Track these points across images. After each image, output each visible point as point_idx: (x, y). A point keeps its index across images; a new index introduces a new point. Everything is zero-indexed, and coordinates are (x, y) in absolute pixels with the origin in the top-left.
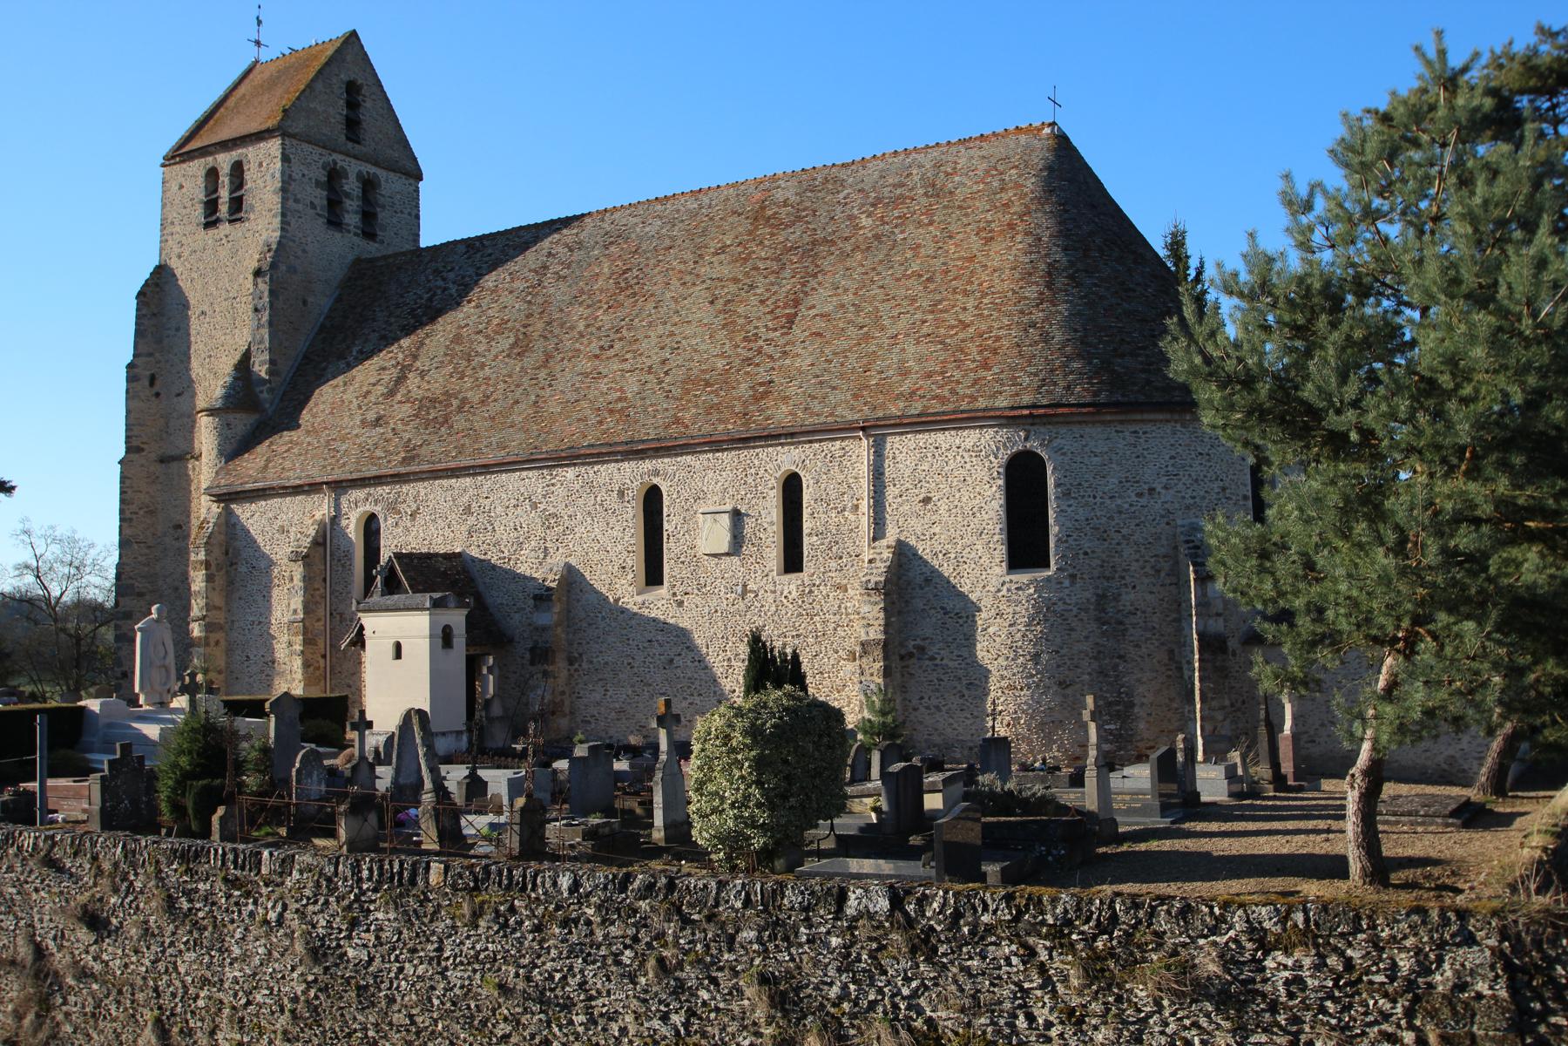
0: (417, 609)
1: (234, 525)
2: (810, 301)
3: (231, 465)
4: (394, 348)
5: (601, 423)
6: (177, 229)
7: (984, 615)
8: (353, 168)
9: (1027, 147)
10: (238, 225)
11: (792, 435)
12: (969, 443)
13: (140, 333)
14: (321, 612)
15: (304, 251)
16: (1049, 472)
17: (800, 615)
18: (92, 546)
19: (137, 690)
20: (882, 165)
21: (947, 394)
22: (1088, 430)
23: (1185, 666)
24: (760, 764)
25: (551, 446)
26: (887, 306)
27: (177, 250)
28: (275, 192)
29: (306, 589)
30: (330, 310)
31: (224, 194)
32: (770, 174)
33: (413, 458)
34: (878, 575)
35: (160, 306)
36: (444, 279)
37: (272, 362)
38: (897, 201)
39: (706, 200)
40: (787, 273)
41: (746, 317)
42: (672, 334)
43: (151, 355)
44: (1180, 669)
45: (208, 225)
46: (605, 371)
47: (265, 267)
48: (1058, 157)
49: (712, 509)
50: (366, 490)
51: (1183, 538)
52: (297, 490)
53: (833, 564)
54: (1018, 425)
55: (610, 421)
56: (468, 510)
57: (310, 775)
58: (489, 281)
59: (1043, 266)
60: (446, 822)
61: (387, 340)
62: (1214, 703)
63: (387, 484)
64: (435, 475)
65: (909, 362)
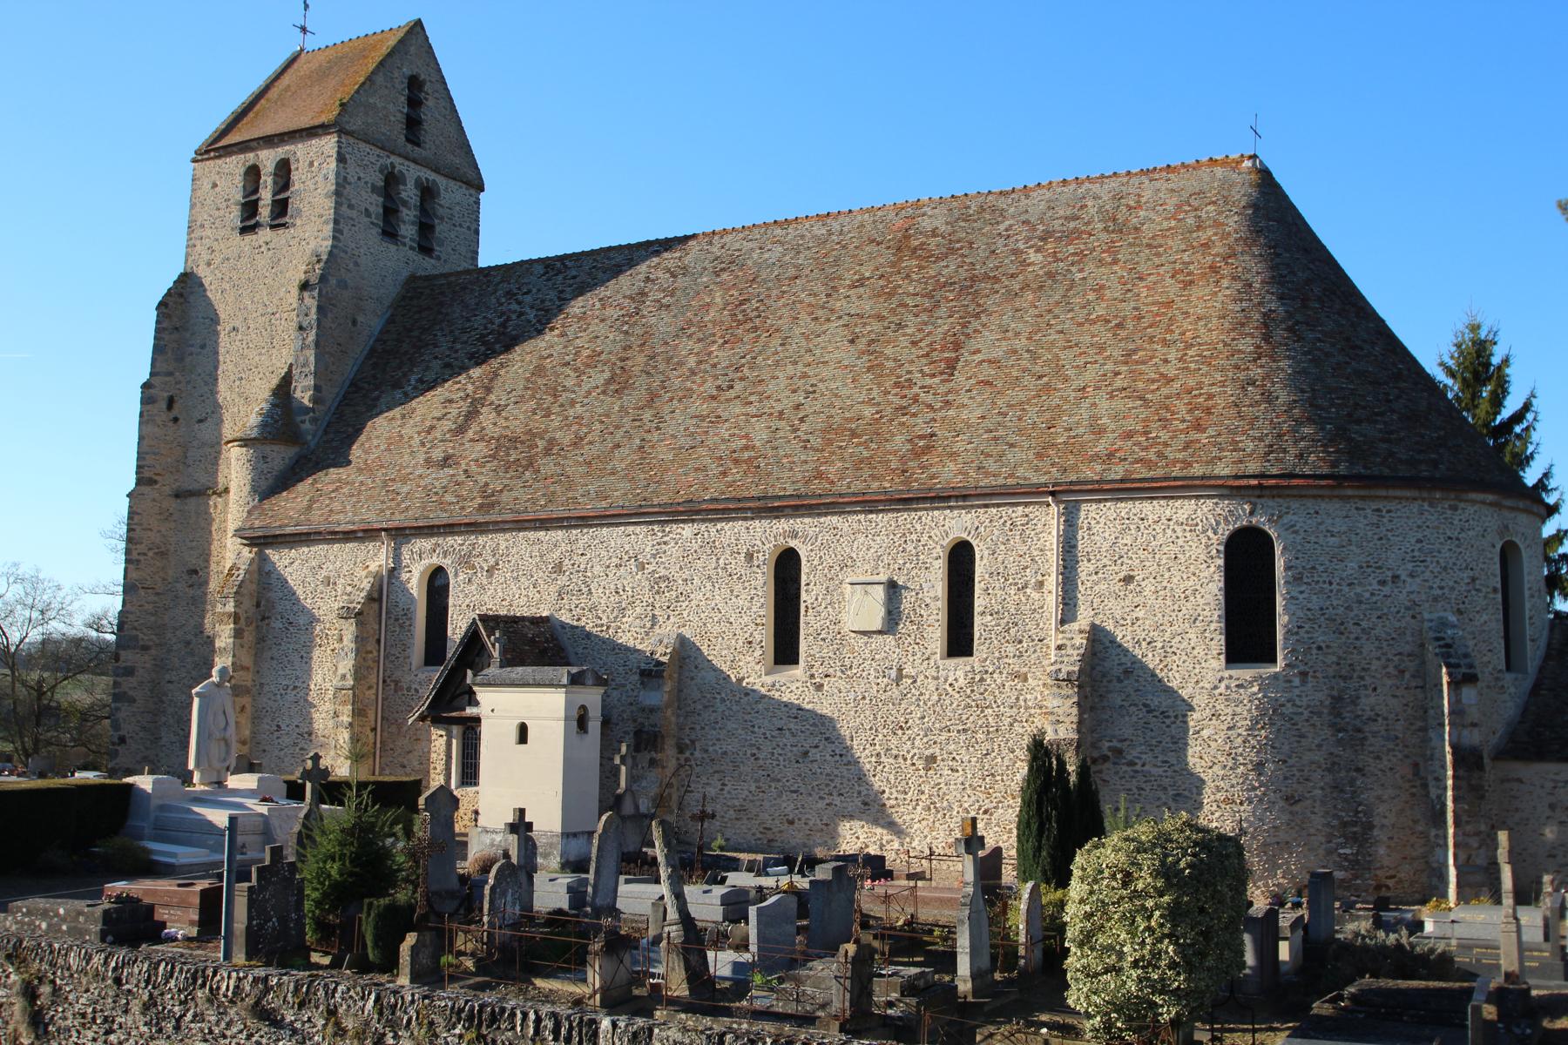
0: (551, 685)
1: (269, 573)
2: (973, 344)
3: (267, 504)
4: (462, 378)
5: (724, 474)
6: (208, 232)
7: (1196, 716)
8: (413, 173)
9: (1224, 181)
10: (281, 231)
11: (965, 497)
12: (1182, 515)
13: (158, 349)
14: (372, 679)
15: (356, 264)
16: (1278, 552)
17: (968, 706)
18: (59, 588)
19: (191, 766)
20: (1048, 195)
21: (1154, 458)
22: (1323, 505)
23: (1432, 783)
24: (1174, 914)
25: (664, 499)
26: (1070, 354)
27: (206, 256)
28: (327, 196)
29: (358, 651)
30: (381, 332)
31: (266, 196)
32: (912, 199)
33: (492, 505)
34: (1071, 663)
35: (184, 318)
36: (519, 303)
37: (317, 388)
38: (1071, 236)
39: (836, 226)
40: (943, 311)
41: (895, 360)
42: (805, 376)
43: (170, 374)
44: (1425, 786)
45: (245, 230)
46: (725, 415)
47: (314, 280)
48: (1262, 193)
49: (862, 579)
50: (433, 540)
51: (1432, 634)
52: (348, 536)
53: (1011, 649)
54: (1243, 497)
55: (736, 473)
56: (558, 568)
57: (504, 894)
58: (576, 307)
59: (1257, 316)
60: (693, 959)
61: (452, 369)
62: (1468, 828)
63: (460, 533)
64: (520, 525)
65: (1101, 417)
